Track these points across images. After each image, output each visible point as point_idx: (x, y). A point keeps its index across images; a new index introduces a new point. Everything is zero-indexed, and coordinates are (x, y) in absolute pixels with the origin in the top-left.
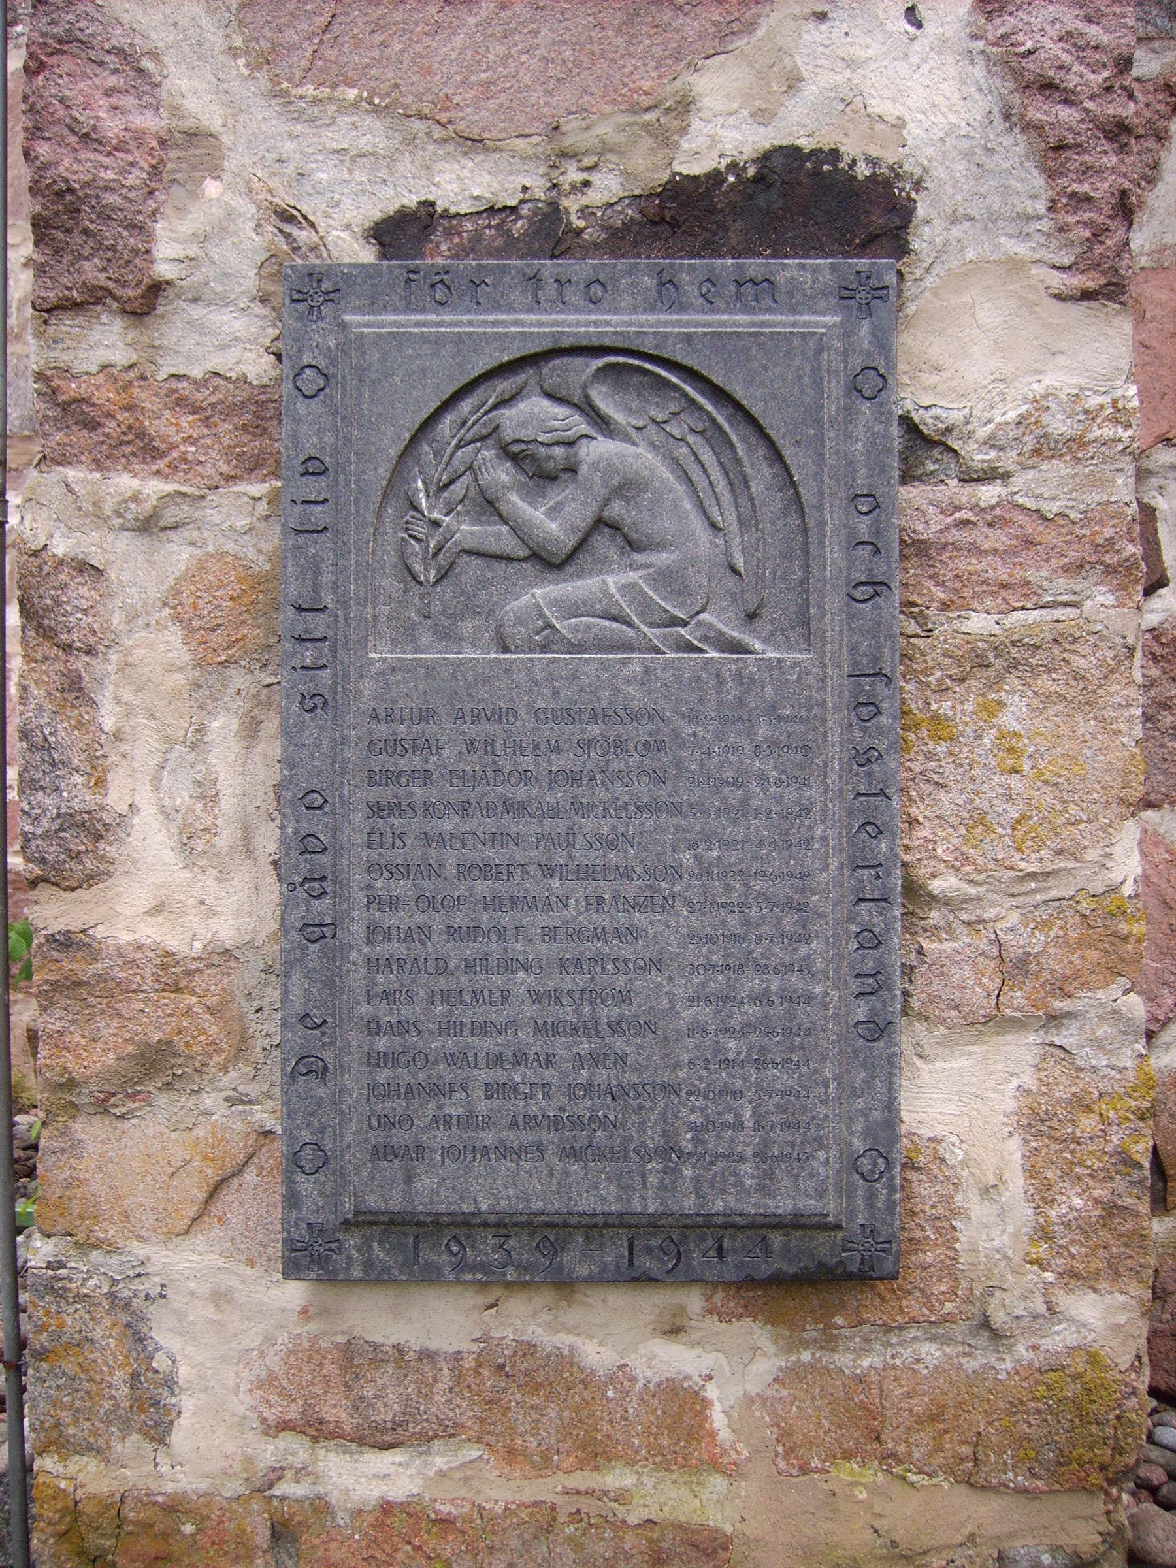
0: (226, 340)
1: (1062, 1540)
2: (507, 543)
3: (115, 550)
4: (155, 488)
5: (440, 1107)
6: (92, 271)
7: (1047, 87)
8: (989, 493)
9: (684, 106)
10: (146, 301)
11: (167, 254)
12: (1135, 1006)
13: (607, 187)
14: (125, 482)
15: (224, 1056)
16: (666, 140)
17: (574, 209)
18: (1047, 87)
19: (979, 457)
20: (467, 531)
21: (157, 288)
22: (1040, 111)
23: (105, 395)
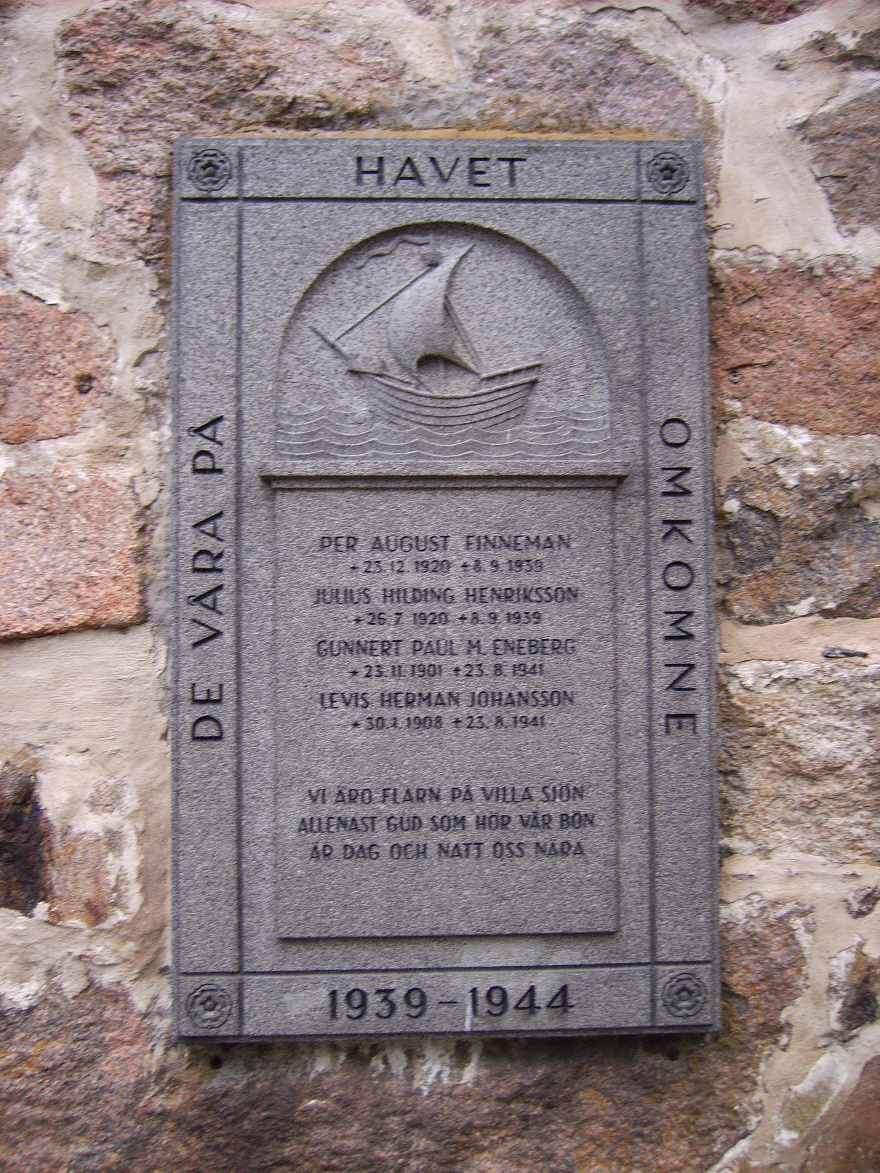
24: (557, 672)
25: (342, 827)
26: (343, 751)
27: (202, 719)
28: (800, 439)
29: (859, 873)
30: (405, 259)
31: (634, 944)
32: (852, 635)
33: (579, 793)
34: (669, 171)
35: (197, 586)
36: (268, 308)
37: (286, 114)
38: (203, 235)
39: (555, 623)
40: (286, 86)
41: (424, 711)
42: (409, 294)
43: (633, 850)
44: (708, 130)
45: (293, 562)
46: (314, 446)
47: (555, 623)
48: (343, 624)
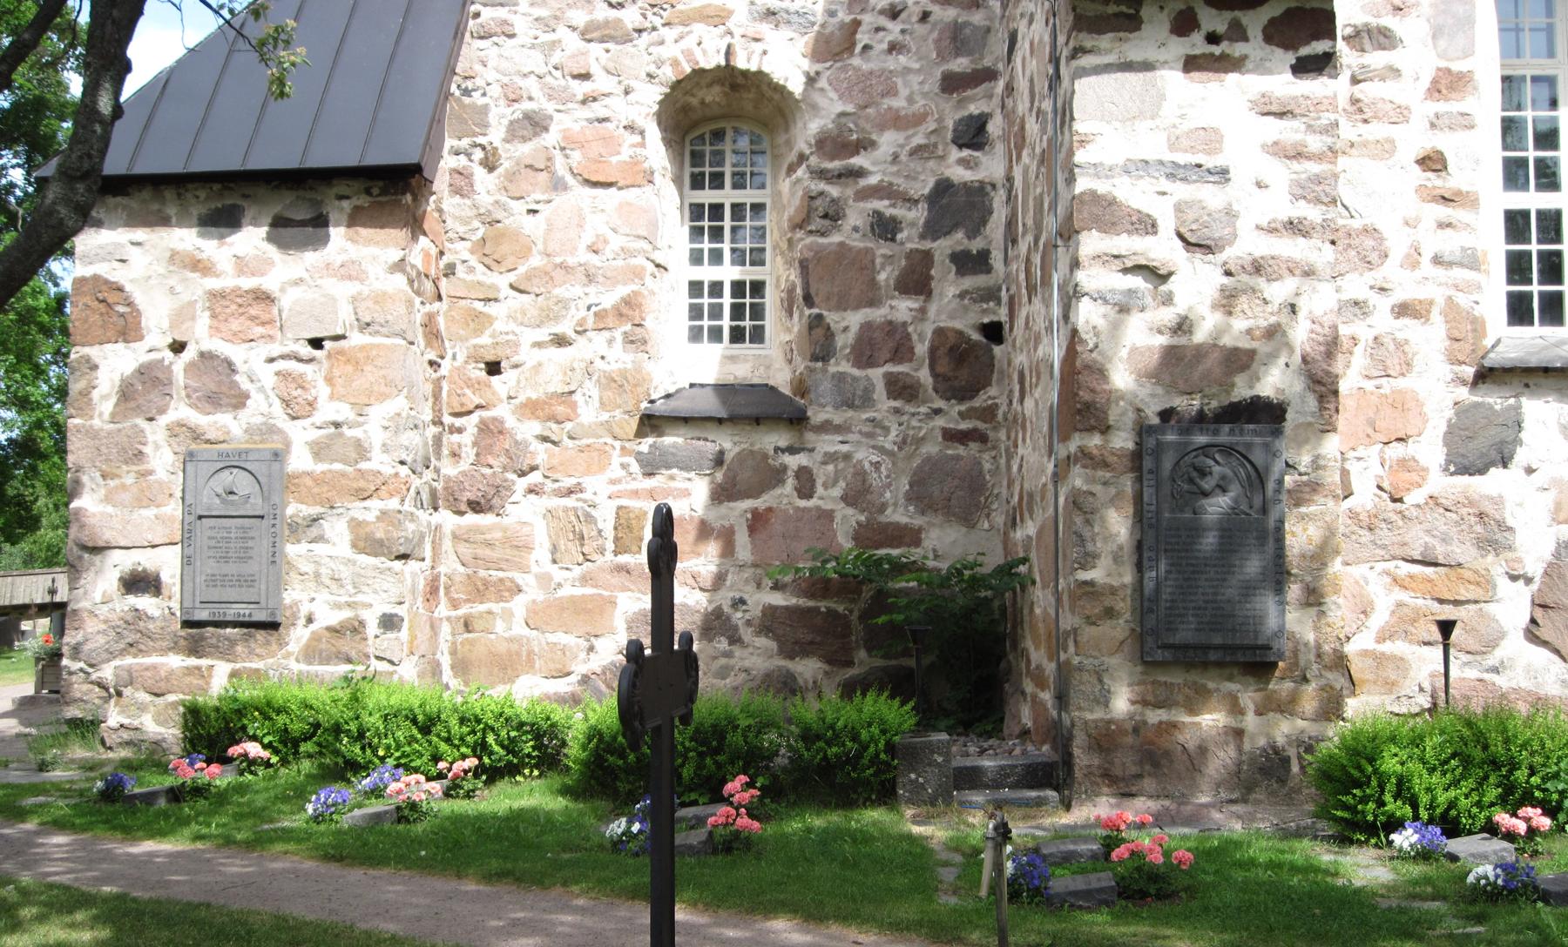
0: (1123, 441)
1: (896, 818)
2: (1195, 489)
3: (1098, 489)
4: (1108, 475)
5: (860, 711)
6: (1092, 422)
7: (1319, 382)
8: (1305, 478)
9: (1233, 385)
10: (1105, 430)
11: (1112, 419)
12: (743, 778)
13: (1214, 404)
14: (1100, 473)
15: (621, 762)
16: (1228, 393)
17: (520, 629)
18: (1319, 382)
19: (1303, 470)
20: (1186, 487)
21: (1109, 427)
22: (1318, 388)
23: (1095, 452)
24: (251, 552)
25: (212, 581)
26: (211, 567)
27: (187, 561)
28: (303, 507)
29: (1034, 26)
30: (227, 472)
31: (263, 604)
32: (313, 546)
33: (343, 337)
34: (276, 454)
35: (187, 538)
36: (201, 481)
37: (208, 441)
38: (189, 466)
39: (250, 544)
40: (207, 437)
41: (226, 559)
42: (227, 478)
43: (263, 587)
44: (288, 444)
45: (205, 528)
46: (209, 509)
47: (250, 544)
48: (213, 543)
